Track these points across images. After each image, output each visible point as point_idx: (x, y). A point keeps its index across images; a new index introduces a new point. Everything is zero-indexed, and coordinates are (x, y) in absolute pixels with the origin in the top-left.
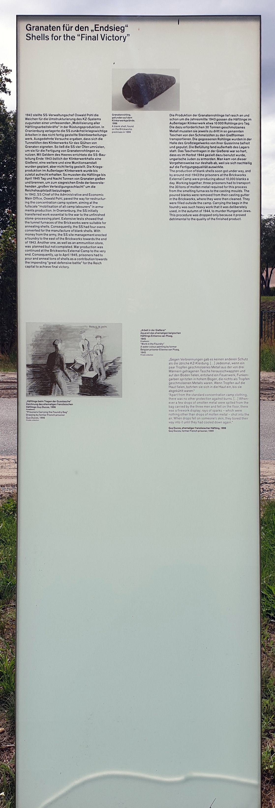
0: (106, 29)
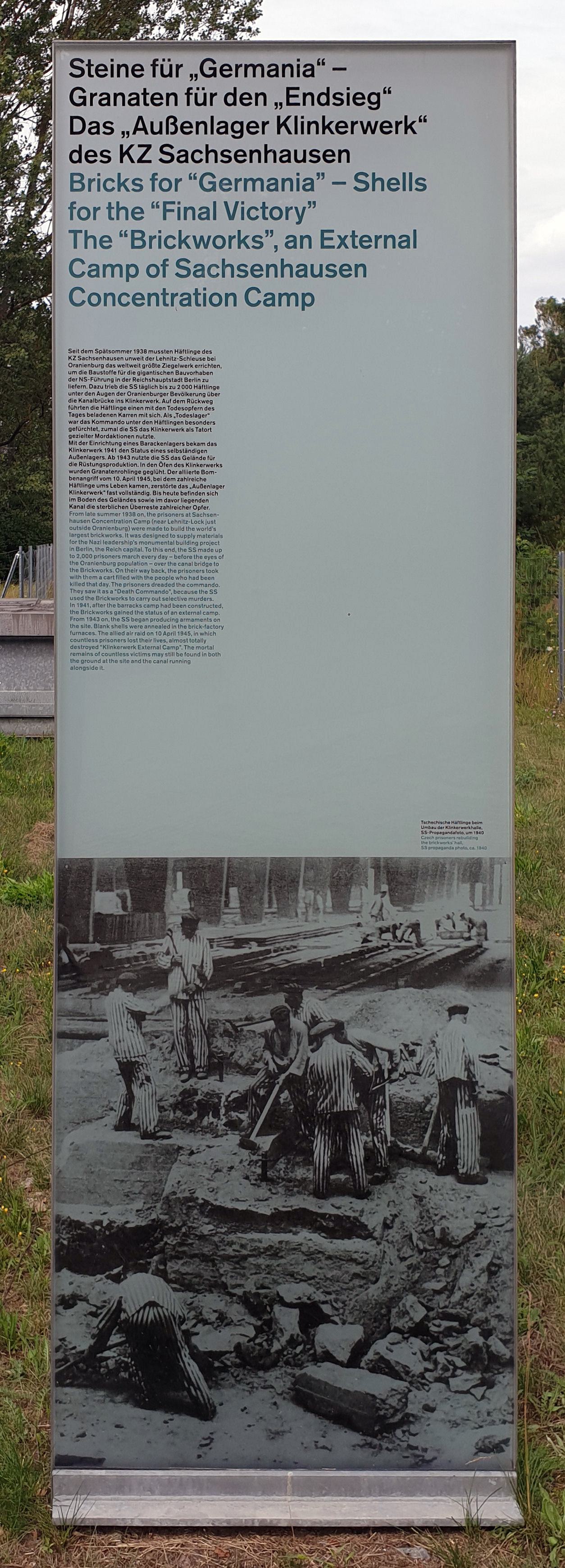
0: (323, 99)
